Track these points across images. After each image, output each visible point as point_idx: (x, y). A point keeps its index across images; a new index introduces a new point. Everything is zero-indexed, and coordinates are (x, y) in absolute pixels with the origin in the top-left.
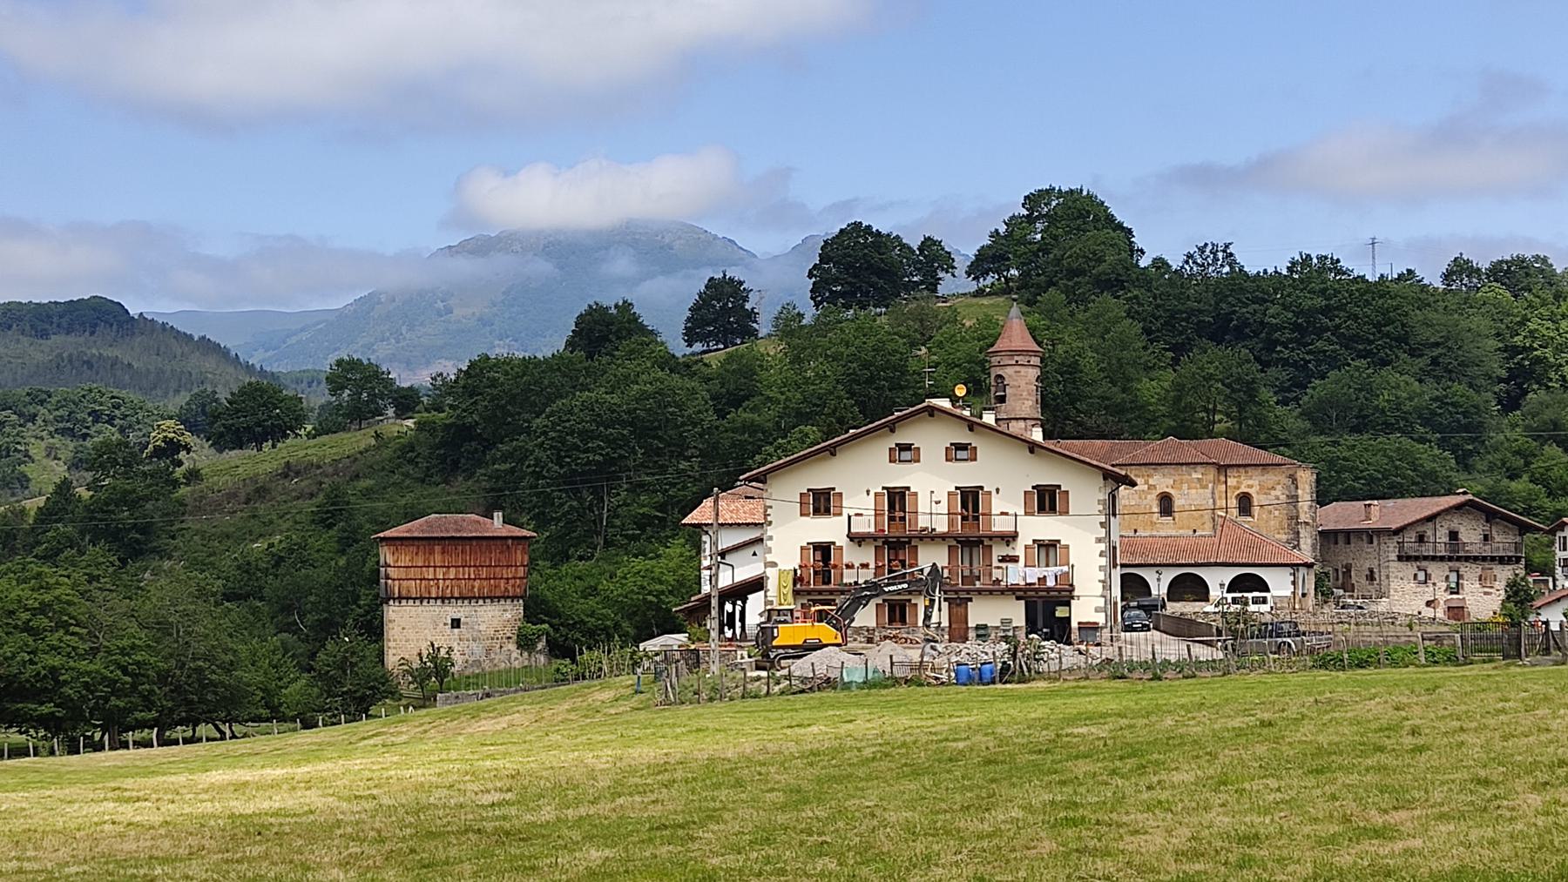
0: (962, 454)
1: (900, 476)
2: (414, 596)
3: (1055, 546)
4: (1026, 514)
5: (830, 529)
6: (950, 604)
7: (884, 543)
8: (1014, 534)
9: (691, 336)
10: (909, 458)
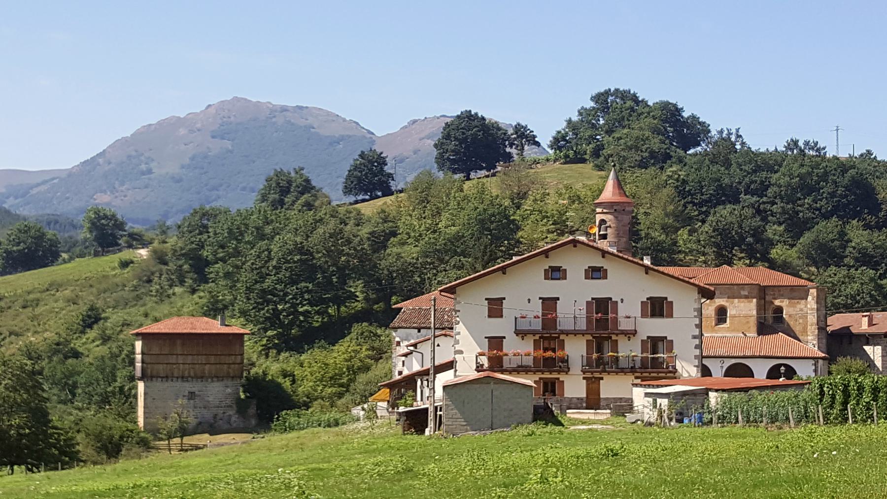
0: (596, 274)
1: (551, 289)
2: (162, 376)
3: (663, 341)
4: (642, 317)
5: (502, 327)
6: (587, 381)
7: (540, 337)
8: (634, 332)
9: (347, 191)
10: (558, 277)
